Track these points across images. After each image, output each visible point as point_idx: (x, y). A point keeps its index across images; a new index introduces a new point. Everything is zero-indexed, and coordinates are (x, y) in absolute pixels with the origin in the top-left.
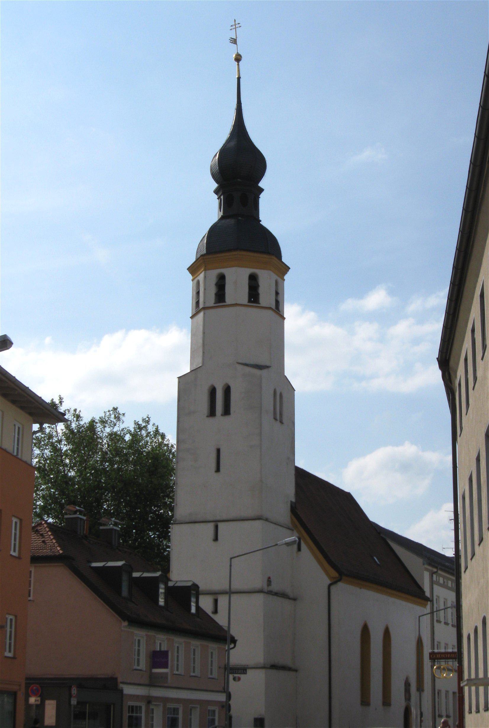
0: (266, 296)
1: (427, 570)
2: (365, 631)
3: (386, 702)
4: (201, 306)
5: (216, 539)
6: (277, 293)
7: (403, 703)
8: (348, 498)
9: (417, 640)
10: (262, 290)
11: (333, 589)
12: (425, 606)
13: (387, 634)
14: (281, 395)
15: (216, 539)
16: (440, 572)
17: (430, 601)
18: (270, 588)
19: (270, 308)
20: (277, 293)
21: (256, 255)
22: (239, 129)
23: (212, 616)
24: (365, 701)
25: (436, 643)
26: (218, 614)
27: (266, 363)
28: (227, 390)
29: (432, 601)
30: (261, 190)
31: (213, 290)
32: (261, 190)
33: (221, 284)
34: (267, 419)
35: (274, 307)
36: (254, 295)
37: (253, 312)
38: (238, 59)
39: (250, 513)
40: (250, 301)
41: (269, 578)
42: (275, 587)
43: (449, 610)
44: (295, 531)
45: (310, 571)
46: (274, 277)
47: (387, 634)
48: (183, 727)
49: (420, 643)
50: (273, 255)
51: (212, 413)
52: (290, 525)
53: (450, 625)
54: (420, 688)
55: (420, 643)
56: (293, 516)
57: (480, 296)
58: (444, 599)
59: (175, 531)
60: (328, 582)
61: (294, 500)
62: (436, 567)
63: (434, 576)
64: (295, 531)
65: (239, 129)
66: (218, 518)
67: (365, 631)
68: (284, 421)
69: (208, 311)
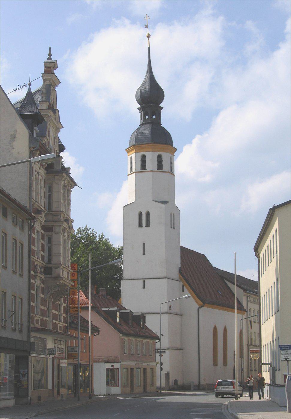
0: (166, 167)
1: (245, 295)
3: (225, 363)
4: (134, 171)
5: (144, 287)
6: (171, 163)
8: (203, 257)
9: (240, 332)
10: (164, 163)
11: (200, 309)
12: (243, 314)
13: (225, 330)
14: (174, 215)
15: (144, 287)
16: (251, 295)
18: (171, 311)
19: (168, 172)
20: (171, 163)
21: (161, 145)
23: (252, 400)
24: (215, 363)
25: (249, 333)
27: (166, 201)
28: (148, 214)
29: (247, 311)
30: (162, 108)
31: (140, 163)
32: (162, 108)
33: (143, 159)
35: (170, 171)
36: (160, 166)
37: (160, 175)
38: (149, 36)
39: (162, 276)
41: (170, 306)
42: (172, 311)
43: (256, 317)
44: (181, 282)
46: (170, 155)
47: (225, 330)
48: (2, 338)
50: (169, 145)
51: (140, 225)
52: (179, 279)
53: (257, 323)
56: (180, 275)
57: (276, 269)
58: (254, 309)
59: (123, 283)
60: (198, 307)
61: (180, 267)
62: (250, 294)
63: (249, 297)
64: (181, 282)
66: (144, 277)
68: (175, 228)
69: (137, 174)
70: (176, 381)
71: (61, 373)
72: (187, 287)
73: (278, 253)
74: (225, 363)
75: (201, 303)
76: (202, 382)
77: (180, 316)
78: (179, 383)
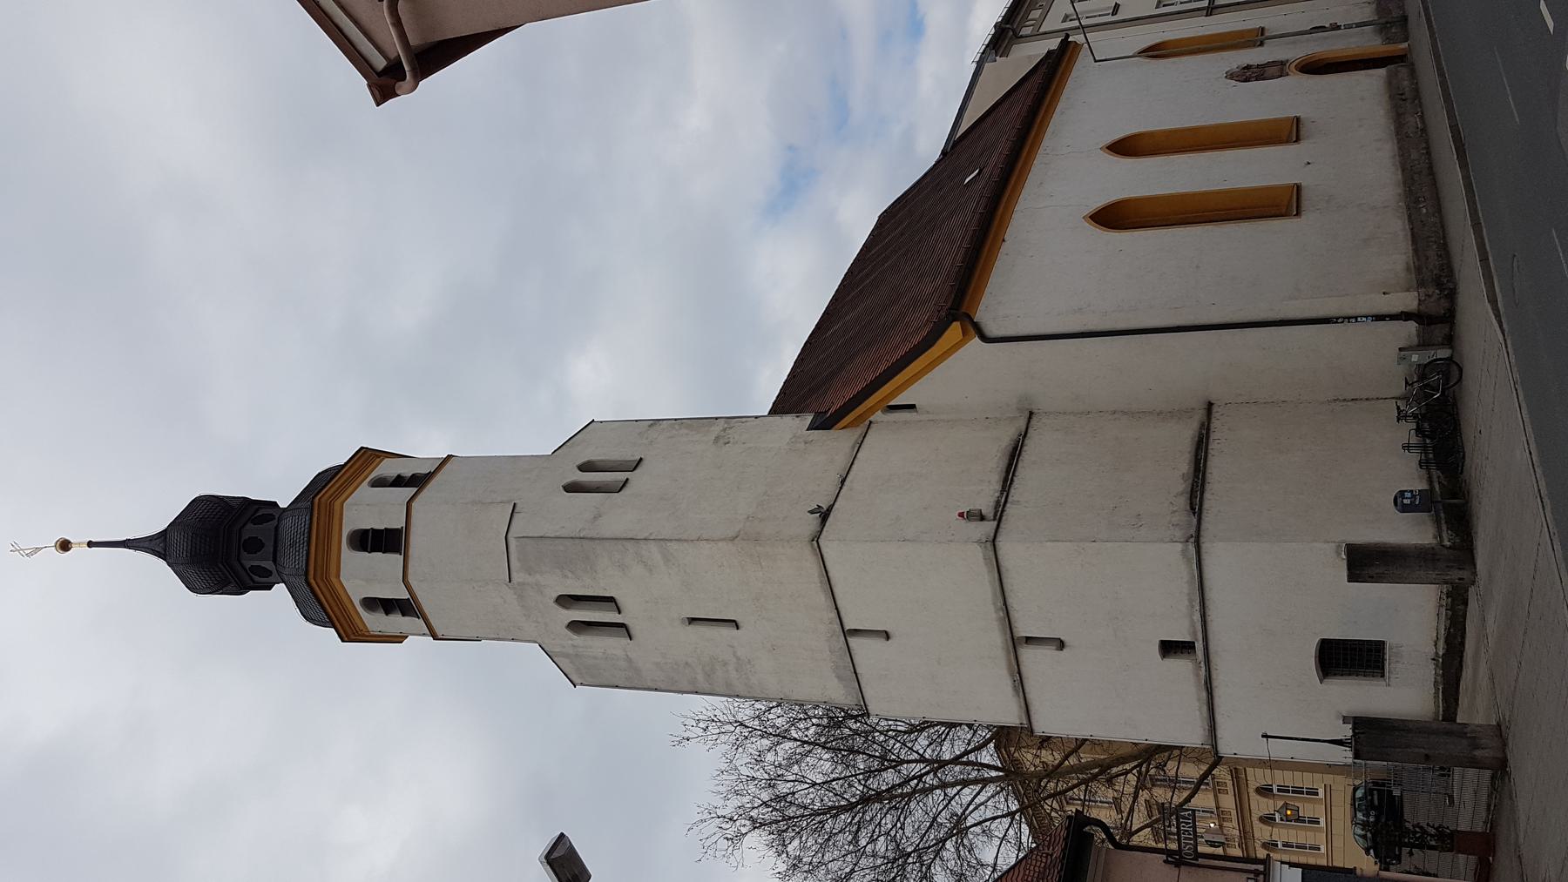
2: (1112, 217)
3: (1288, 132)
7: (1296, 81)
11: (992, 329)
13: (1124, 147)
14: (585, 467)
17: (1067, 36)
22: (156, 545)
24: (1281, 204)
26: (1302, 116)
34: (617, 514)
35: (409, 491)
37: (418, 542)
40: (397, 550)
45: (959, 378)
47: (1124, 147)
49: (1155, 52)
52: (859, 431)
54: (1257, 38)
55: (1155, 52)
65: (156, 545)
67: (1112, 217)
70: (1403, 503)
71: (1191, 615)
72: (893, 394)
73: (1523, 405)
74: (1288, 132)
75: (955, 329)
76: (1408, 301)
77: (1034, 422)
78: (1409, 476)
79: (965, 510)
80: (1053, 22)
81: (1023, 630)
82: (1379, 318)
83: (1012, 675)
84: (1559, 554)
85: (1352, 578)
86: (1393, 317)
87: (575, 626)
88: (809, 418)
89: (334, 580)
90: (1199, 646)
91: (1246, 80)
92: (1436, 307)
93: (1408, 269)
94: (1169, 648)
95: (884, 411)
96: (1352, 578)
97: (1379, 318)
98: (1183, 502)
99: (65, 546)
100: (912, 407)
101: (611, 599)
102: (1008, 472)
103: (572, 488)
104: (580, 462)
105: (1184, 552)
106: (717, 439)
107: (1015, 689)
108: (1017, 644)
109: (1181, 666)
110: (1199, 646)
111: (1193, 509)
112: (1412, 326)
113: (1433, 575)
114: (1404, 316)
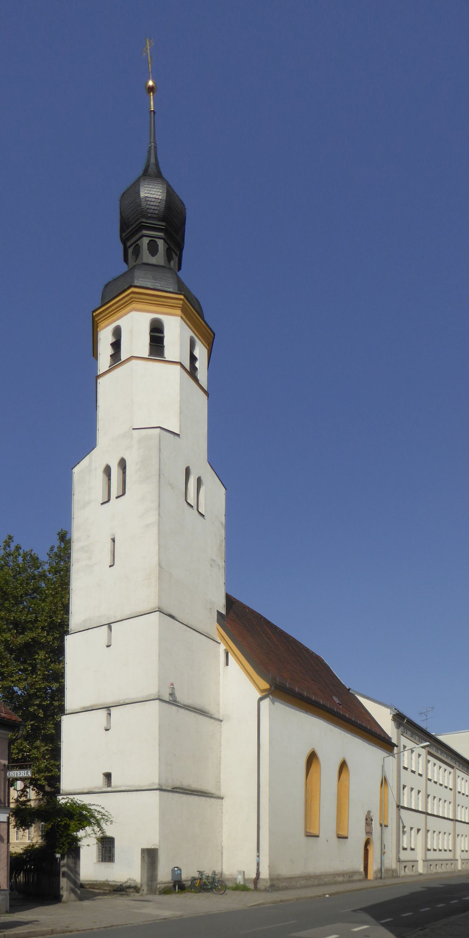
7: (363, 838)
17: (397, 746)
37: (156, 367)
40: (152, 353)
49: (384, 781)
54: (383, 826)
55: (384, 781)
70: (176, 872)
79: (175, 686)
80: (404, 741)
81: (113, 711)
82: (258, 864)
83: (91, 707)
84: (157, 921)
85: (143, 851)
86: (258, 870)
87: (108, 471)
88: (223, 612)
89: (134, 305)
90: (109, 789)
91: (366, 820)
92: (261, 885)
93: (278, 875)
94: (108, 776)
95: (225, 650)
96: (143, 851)
97: (258, 864)
98: (178, 784)
99: (88, 845)
100: (227, 664)
101: (124, 493)
102: (193, 708)
103: (188, 471)
104: (203, 479)
105: (154, 784)
106: (213, 560)
107: (84, 708)
108: (108, 708)
109: (99, 782)
110: (109, 789)
111: (174, 788)
112: (254, 876)
113: (145, 880)
114: (258, 874)
